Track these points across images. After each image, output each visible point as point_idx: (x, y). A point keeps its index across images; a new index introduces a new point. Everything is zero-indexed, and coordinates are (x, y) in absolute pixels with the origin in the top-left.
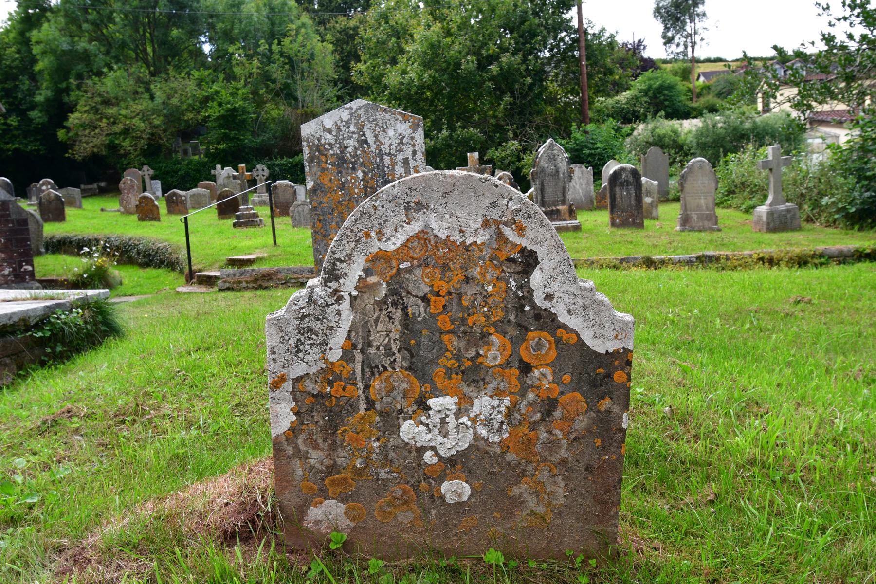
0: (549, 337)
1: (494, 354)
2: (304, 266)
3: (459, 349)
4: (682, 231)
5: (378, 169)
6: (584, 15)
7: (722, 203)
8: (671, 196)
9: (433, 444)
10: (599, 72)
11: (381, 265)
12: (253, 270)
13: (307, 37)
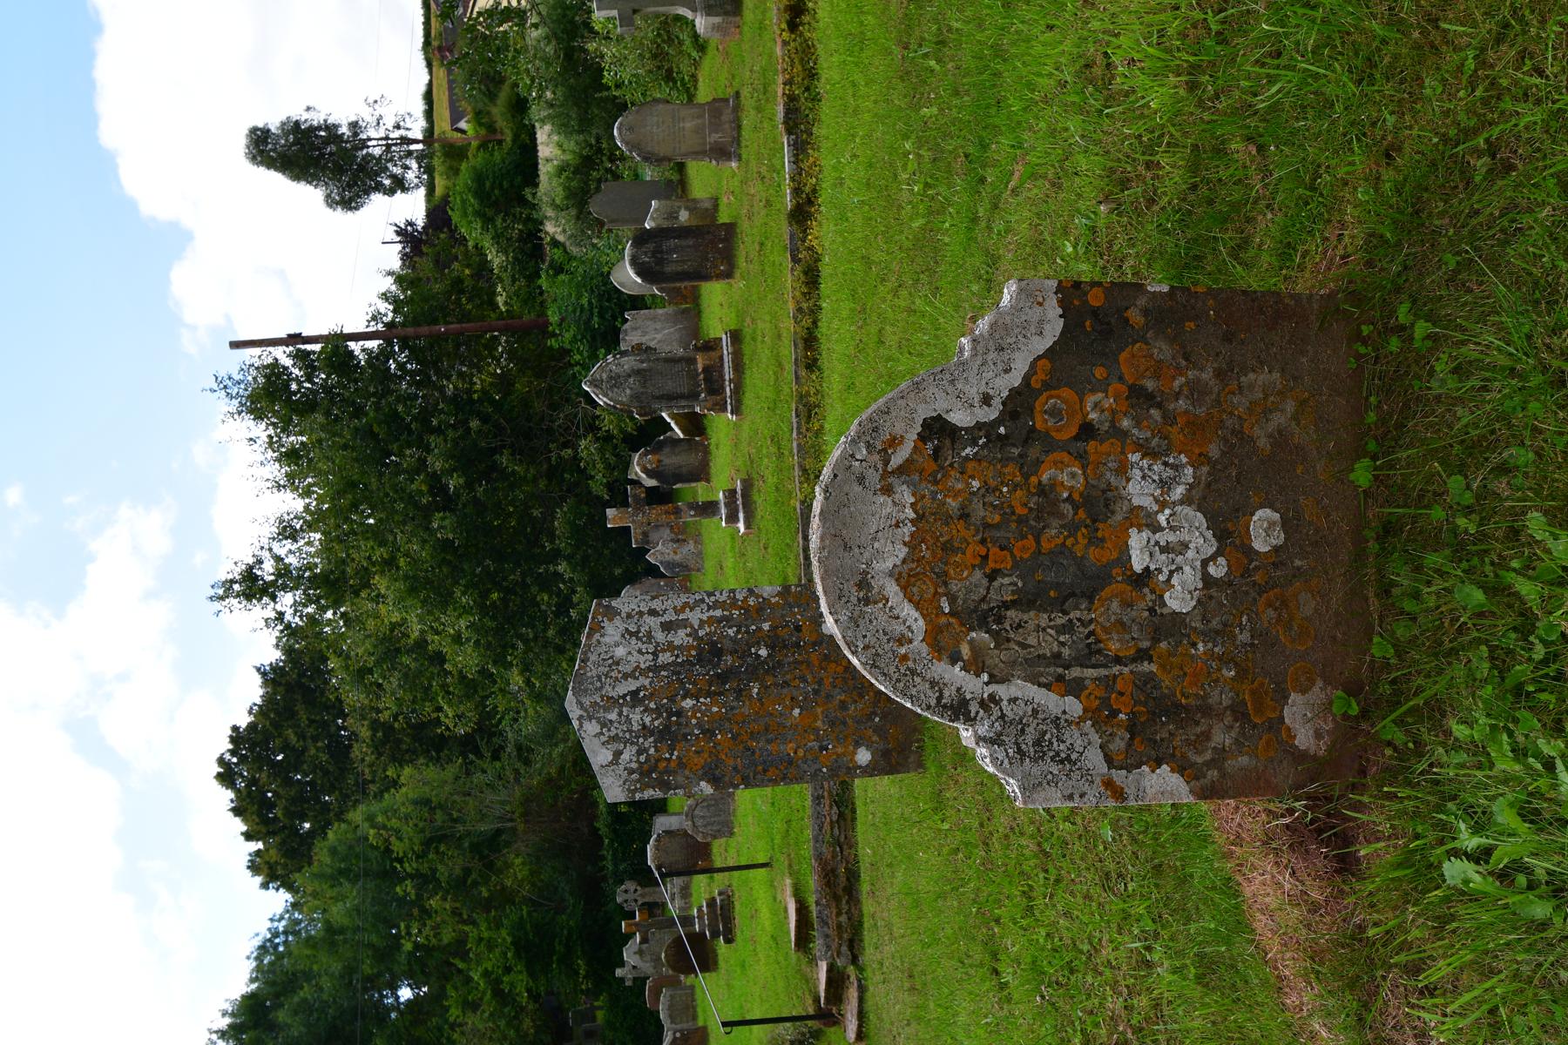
0: (1042, 398)
1: (1068, 477)
2: (809, 812)
3: (1062, 526)
4: (739, 158)
5: (679, 673)
6: (360, 327)
7: (687, 91)
8: (675, 177)
9: (1198, 564)
10: (458, 302)
11: (945, 639)
12: (817, 903)
13: (391, 812)
